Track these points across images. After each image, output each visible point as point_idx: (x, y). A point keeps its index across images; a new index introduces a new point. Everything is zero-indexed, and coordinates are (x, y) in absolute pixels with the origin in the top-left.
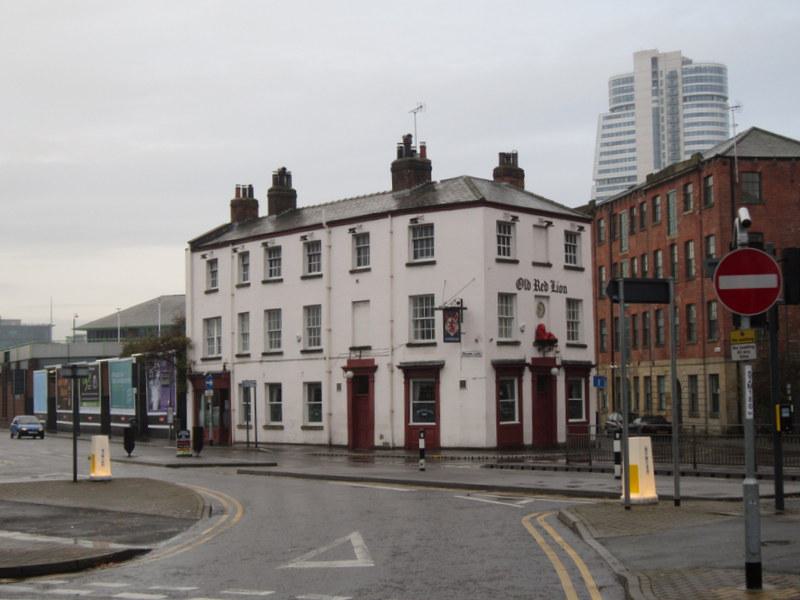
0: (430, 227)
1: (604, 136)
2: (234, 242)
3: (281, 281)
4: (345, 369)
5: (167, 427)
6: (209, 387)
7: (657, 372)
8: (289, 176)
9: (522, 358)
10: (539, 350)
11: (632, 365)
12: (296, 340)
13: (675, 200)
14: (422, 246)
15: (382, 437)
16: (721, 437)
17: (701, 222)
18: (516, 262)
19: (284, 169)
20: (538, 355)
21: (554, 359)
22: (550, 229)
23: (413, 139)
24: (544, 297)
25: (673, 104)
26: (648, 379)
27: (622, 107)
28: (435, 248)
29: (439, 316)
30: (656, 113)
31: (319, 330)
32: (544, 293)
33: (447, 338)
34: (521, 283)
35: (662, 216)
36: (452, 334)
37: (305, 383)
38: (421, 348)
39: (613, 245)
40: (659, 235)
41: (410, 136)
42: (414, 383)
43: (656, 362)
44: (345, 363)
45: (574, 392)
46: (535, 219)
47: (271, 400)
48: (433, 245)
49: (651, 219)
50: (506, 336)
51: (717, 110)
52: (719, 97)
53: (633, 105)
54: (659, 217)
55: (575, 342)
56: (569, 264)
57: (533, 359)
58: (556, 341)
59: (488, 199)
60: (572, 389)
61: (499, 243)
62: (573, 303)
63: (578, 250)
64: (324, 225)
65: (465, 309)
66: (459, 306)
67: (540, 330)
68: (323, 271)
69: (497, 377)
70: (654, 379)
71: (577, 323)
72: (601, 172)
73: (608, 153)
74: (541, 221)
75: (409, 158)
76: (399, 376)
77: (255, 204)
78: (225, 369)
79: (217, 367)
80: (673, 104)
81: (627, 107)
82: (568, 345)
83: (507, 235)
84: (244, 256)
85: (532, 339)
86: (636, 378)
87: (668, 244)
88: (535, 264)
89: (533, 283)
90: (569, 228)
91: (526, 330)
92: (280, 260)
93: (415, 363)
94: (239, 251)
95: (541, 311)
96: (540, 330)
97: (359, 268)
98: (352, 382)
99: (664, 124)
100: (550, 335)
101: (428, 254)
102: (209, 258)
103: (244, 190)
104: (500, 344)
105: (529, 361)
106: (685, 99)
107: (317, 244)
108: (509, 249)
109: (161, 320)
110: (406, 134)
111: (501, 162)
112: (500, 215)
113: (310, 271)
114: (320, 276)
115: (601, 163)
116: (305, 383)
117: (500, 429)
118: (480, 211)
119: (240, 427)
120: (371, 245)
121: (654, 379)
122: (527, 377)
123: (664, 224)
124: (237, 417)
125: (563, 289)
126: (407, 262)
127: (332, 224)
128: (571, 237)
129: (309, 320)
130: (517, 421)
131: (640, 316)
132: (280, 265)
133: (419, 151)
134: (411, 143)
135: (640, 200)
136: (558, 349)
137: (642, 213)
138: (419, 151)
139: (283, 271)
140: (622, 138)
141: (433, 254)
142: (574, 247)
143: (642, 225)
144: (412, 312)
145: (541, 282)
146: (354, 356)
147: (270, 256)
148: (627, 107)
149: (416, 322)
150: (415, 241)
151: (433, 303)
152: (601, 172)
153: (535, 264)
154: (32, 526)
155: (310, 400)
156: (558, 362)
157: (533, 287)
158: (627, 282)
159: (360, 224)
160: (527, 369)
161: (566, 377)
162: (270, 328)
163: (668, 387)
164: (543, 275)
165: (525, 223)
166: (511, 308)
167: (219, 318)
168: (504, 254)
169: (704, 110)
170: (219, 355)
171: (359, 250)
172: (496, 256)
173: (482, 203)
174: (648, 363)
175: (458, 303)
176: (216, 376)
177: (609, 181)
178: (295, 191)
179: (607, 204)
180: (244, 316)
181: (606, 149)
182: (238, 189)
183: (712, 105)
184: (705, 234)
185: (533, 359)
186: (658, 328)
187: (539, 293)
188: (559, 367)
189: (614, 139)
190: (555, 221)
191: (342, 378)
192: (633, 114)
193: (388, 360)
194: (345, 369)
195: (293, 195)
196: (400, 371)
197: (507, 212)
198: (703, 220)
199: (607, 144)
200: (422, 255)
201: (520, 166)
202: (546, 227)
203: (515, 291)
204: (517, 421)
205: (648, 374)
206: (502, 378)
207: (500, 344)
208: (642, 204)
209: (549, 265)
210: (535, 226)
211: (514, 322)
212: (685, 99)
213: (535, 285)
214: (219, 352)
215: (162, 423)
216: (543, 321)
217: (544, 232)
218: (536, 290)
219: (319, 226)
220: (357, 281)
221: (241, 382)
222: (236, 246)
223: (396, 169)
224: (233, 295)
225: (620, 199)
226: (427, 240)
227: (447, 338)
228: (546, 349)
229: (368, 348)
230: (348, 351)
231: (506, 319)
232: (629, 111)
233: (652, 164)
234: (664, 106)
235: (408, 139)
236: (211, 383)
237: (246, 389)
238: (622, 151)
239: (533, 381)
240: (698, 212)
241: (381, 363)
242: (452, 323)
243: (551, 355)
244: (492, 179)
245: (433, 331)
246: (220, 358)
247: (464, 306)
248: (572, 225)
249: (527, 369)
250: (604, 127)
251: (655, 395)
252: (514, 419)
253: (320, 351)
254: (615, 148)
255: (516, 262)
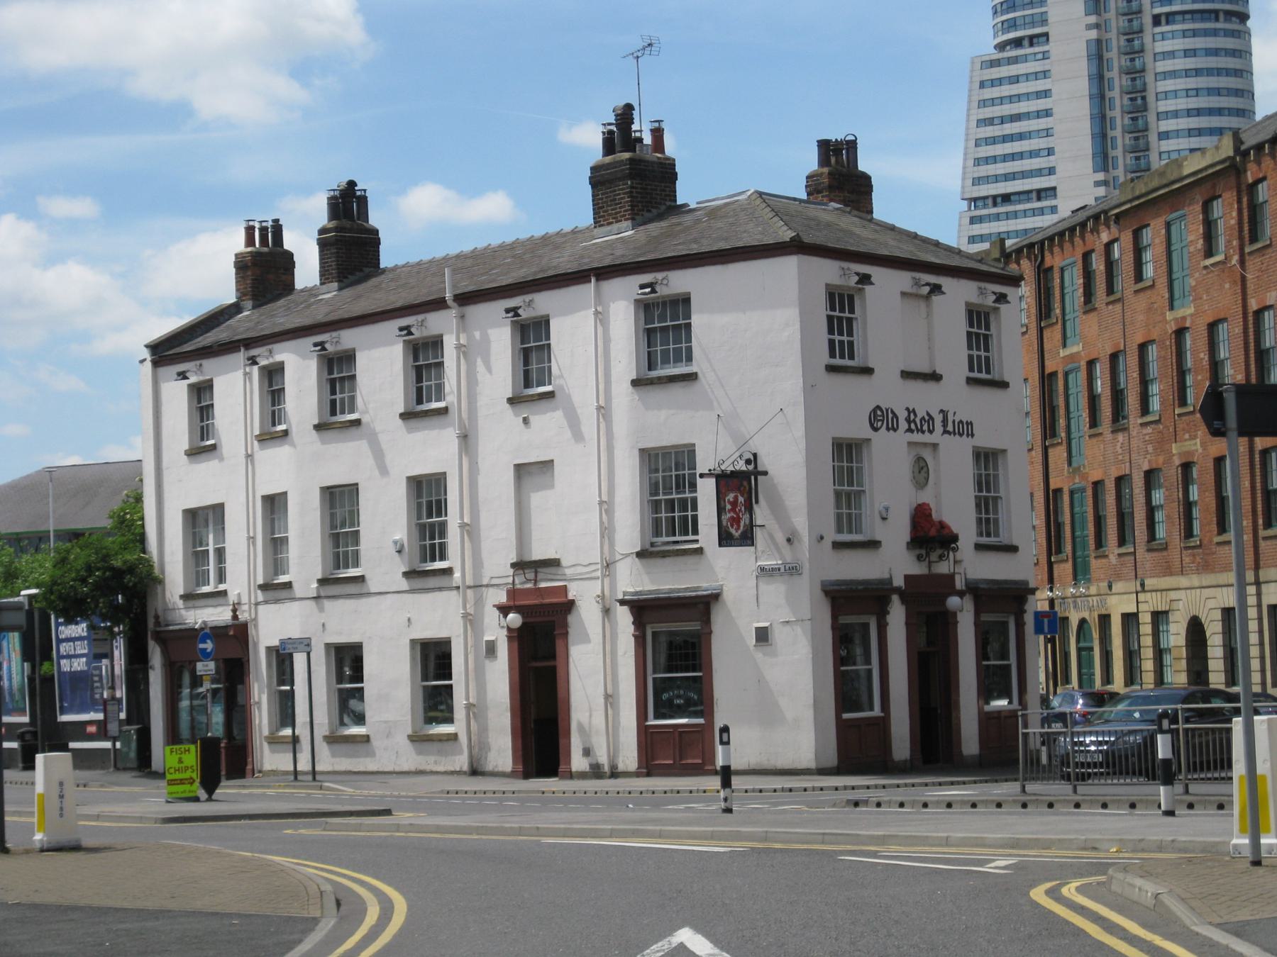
0: (683, 302)
1: (983, 103)
2: (249, 343)
3: (691, 377)
4: (504, 610)
5: (107, 745)
6: (205, 655)
7: (1151, 602)
8: (363, 201)
9: (886, 576)
10: (919, 558)
11: (1093, 590)
12: (392, 550)
13: (1190, 232)
14: (665, 342)
15: (587, 752)
16: (822, 772)
17: (1243, 279)
18: (868, 371)
19: (352, 184)
20: (917, 569)
21: (951, 578)
22: (936, 299)
23: (636, 114)
24: (925, 445)
25: (1132, 34)
26: (1130, 620)
27: (1216, 12)
28: (694, 343)
29: (706, 491)
30: (1098, 54)
31: (443, 526)
32: (926, 438)
33: (725, 539)
34: (880, 418)
35: (1155, 269)
36: (736, 534)
37: (413, 642)
38: (668, 560)
39: (1046, 334)
40: (1150, 309)
41: (629, 108)
42: (655, 634)
43: (1147, 582)
44: (502, 598)
45: (994, 647)
46: (903, 280)
47: (340, 679)
48: (689, 340)
49: (1132, 274)
50: (850, 532)
51: (1229, 43)
52: (1229, 14)
53: (1046, 35)
54: (1149, 271)
55: (992, 540)
56: (976, 375)
57: (907, 578)
58: (955, 538)
59: (807, 239)
60: (987, 639)
61: (831, 331)
62: (987, 459)
63: (994, 343)
64: (450, 302)
65: (765, 473)
66: (751, 467)
67: (921, 516)
68: (450, 399)
69: (835, 617)
70: (1146, 618)
71: (996, 499)
72: (977, 181)
73: (993, 141)
74: (917, 283)
75: (627, 155)
76: (624, 617)
77: (286, 262)
78: (235, 617)
79: (218, 615)
80: (1132, 34)
81: (1032, 40)
82: (979, 547)
83: (847, 315)
84: (273, 374)
85: (905, 534)
86: (1105, 620)
87: (1172, 327)
88: (906, 375)
89: (902, 415)
90: (974, 298)
91: (891, 516)
92: (353, 377)
93: (852, 582)
94: (263, 362)
95: (921, 471)
96: (921, 516)
97: (654, 374)
98: (517, 637)
99: (1114, 74)
100: (942, 525)
101: (678, 359)
102: (193, 379)
103: (263, 230)
104: (837, 545)
105: (899, 582)
106: (1157, 20)
107: (436, 344)
108: (851, 344)
109: (96, 517)
110: (622, 103)
111: (824, 160)
112: (830, 272)
113: (527, 384)
114: (444, 411)
115: (978, 162)
116: (413, 642)
117: (842, 727)
118: (790, 265)
119: (273, 740)
120: (553, 341)
121: (1146, 618)
122: (897, 615)
123: (1162, 283)
124: (262, 716)
125: (965, 429)
126: (903, 369)
127: (466, 299)
128: (978, 318)
129: (419, 505)
130: (877, 712)
131: (1110, 486)
132: (353, 389)
133: (648, 139)
134: (630, 121)
135: (1105, 237)
136: (959, 555)
137: (1110, 264)
138: (648, 139)
139: (359, 402)
140: (1023, 107)
141: (689, 359)
142: (986, 337)
143: (1110, 290)
144: (647, 486)
145: (921, 413)
146: (523, 583)
147: (330, 372)
148: (1032, 40)
149: (656, 506)
150: (650, 333)
151: (693, 466)
152: (977, 181)
153: (906, 375)
154: (1165, 881)
155: (425, 677)
156: (959, 584)
157: (903, 425)
158: (1241, 390)
159: (528, 298)
160: (895, 599)
161: (977, 612)
162: (419, 517)
163: (1176, 636)
164: (925, 399)
165: (888, 283)
166: (860, 470)
167: (218, 510)
168: (842, 357)
169: (1211, 42)
170: (222, 587)
171: (419, 371)
172: (825, 359)
173: (796, 247)
174: (1133, 586)
175: (748, 462)
176: (218, 633)
177: (995, 200)
178: (376, 232)
179: (1031, 246)
180: (274, 504)
181: (990, 131)
182: (250, 231)
183: (1215, 33)
184: (1253, 305)
185: (907, 578)
186: (1151, 510)
187: (917, 437)
188: (961, 594)
189: (1007, 109)
190: (946, 282)
191: (496, 629)
192: (1045, 56)
193: (596, 588)
194: (504, 610)
195: (371, 241)
196: (625, 609)
197: (845, 265)
198: (1249, 276)
199: (989, 122)
200: (666, 361)
201: (863, 166)
202: (927, 297)
203: (866, 432)
204: (877, 712)
205: (1131, 609)
206: (985, 617)
207: (837, 545)
208: (1108, 246)
209: (935, 377)
210: (904, 294)
211: (866, 500)
212: (1157, 20)
213: (908, 421)
214: (221, 577)
215: (91, 738)
216: (926, 497)
217: (922, 304)
218: (909, 430)
219: (438, 304)
220: (526, 421)
221: (276, 643)
222: (254, 352)
223: (600, 179)
224: (249, 457)
225: (1061, 234)
226: (677, 328)
227: (725, 539)
228: (934, 556)
229: (554, 563)
230: (511, 571)
231: (848, 495)
232: (1036, 49)
233: (1089, 163)
234: (1113, 35)
235: (625, 115)
236: (209, 646)
237: (282, 659)
238: (1021, 136)
239: (908, 624)
240: (1235, 260)
241: (586, 596)
242: (734, 504)
243: (943, 568)
244: (804, 196)
245: (695, 519)
246: (224, 593)
247: (760, 468)
248: (982, 292)
249: (895, 599)
250: (982, 85)
251: (1147, 653)
252: (872, 709)
253: (448, 572)
254: (1010, 128)
255: (868, 371)
